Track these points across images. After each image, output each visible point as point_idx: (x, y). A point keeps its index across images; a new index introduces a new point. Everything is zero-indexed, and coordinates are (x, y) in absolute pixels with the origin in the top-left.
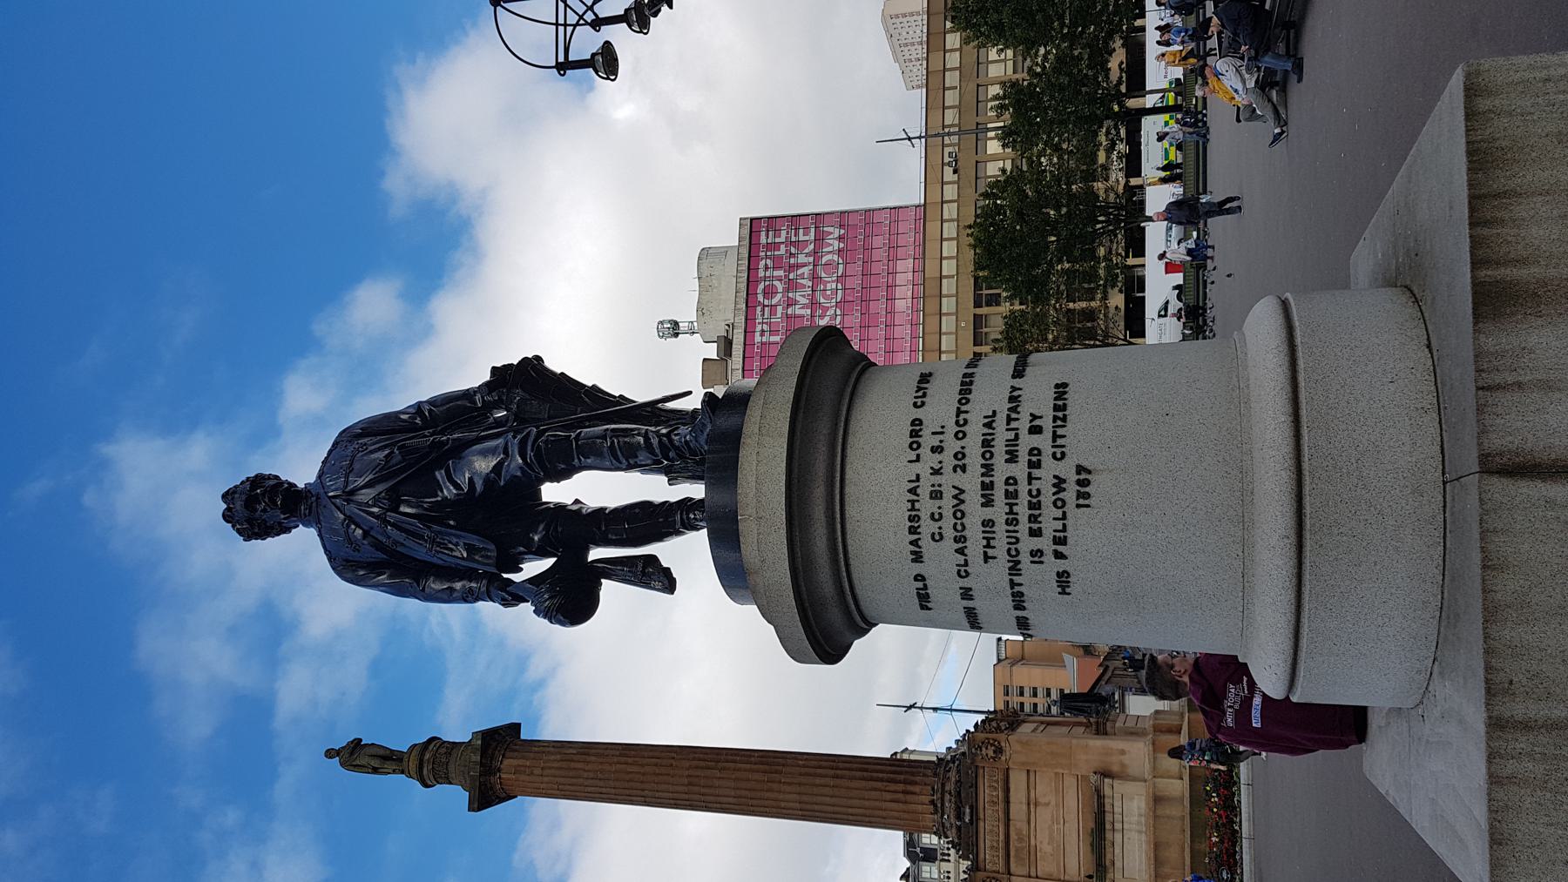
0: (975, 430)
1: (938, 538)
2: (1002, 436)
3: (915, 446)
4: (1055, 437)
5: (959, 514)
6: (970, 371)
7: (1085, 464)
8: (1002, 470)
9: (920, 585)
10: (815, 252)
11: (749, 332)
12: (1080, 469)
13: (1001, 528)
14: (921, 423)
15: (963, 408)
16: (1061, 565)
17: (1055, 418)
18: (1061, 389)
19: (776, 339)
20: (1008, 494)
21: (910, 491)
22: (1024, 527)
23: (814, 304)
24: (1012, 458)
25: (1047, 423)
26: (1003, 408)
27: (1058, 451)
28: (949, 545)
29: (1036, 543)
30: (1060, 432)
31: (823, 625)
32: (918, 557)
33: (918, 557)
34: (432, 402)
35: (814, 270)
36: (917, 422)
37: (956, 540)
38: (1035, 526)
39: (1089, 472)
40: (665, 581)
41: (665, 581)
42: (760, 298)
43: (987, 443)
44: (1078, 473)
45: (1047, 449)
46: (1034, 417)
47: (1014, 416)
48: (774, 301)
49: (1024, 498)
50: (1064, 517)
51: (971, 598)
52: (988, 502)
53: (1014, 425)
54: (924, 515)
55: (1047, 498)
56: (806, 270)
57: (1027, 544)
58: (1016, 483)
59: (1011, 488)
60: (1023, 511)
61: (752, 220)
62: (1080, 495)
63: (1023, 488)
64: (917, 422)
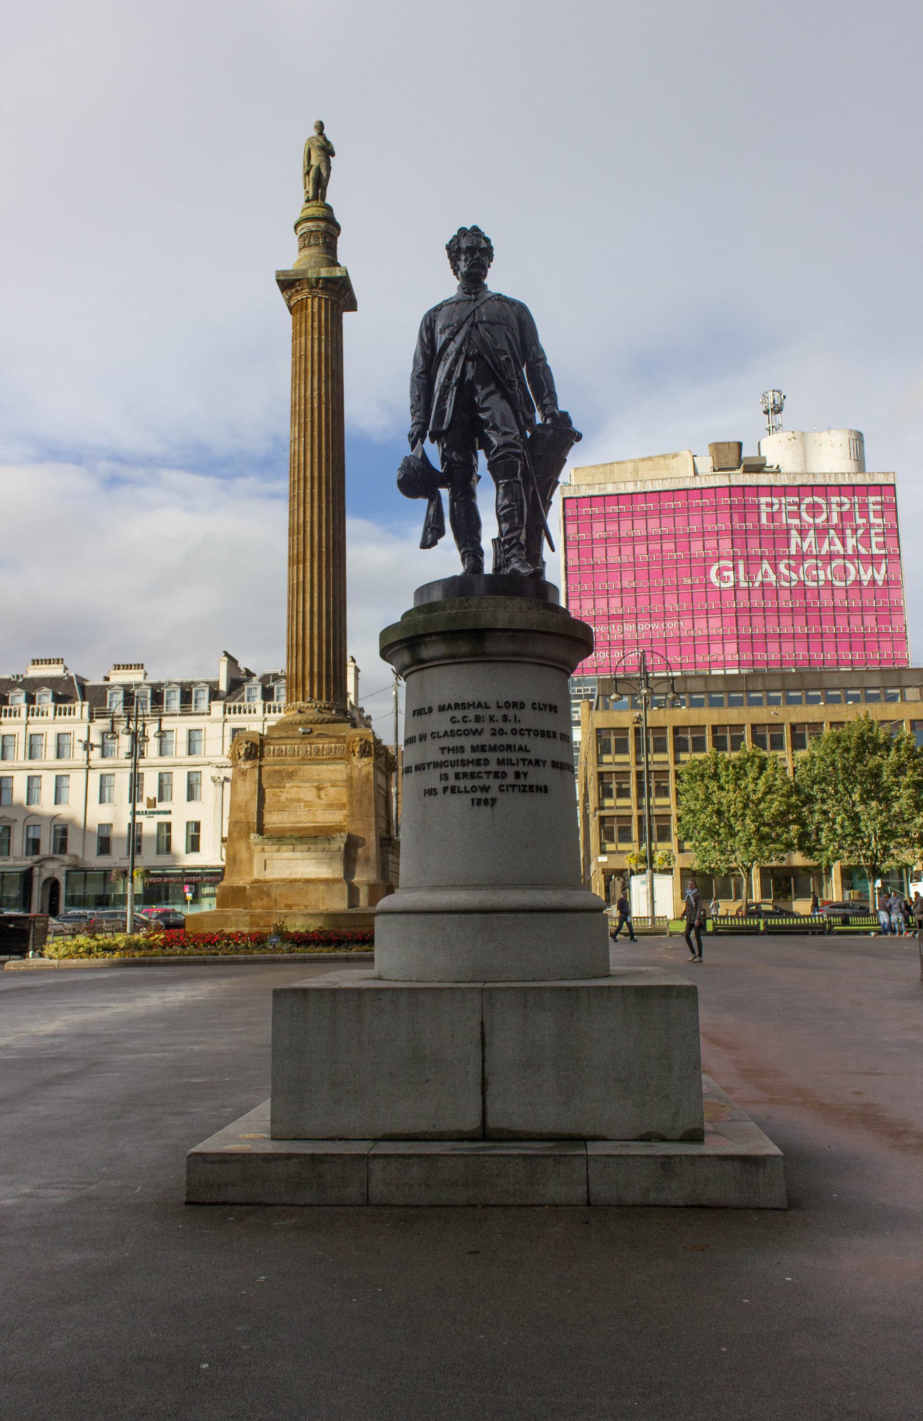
0: (517, 740)
1: (453, 720)
2: (513, 756)
3: (507, 705)
4: (513, 786)
5: (467, 733)
6: (558, 736)
7: (497, 803)
8: (493, 757)
9: (427, 710)
10: (858, 556)
11: (771, 490)
12: (494, 800)
13: (459, 756)
14: (521, 708)
15: (532, 734)
16: (440, 790)
17: (525, 786)
18: (544, 789)
19: (764, 520)
20: (478, 760)
21: (480, 703)
22: (460, 769)
23: (802, 557)
24: (500, 762)
25: (522, 781)
26: (532, 756)
27: (505, 788)
28: (449, 727)
29: (452, 776)
30: (516, 789)
31: (405, 645)
32: (442, 709)
33: (442, 709)
34: (547, 368)
35: (838, 556)
36: (522, 706)
37: (451, 731)
38: (461, 776)
39: (492, 805)
40: (427, 544)
41: (427, 544)
42: (808, 500)
43: (509, 747)
44: (492, 799)
45: (505, 782)
46: (525, 774)
47: (526, 762)
48: (804, 515)
49: (476, 769)
50: (466, 792)
51: (421, 740)
52: (474, 749)
53: (521, 763)
54: (465, 712)
55: (477, 782)
56: (838, 547)
57: (451, 771)
58: (485, 765)
59: (482, 762)
60: (470, 769)
61: (893, 485)
62: (479, 801)
63: (482, 769)
64: (522, 706)
